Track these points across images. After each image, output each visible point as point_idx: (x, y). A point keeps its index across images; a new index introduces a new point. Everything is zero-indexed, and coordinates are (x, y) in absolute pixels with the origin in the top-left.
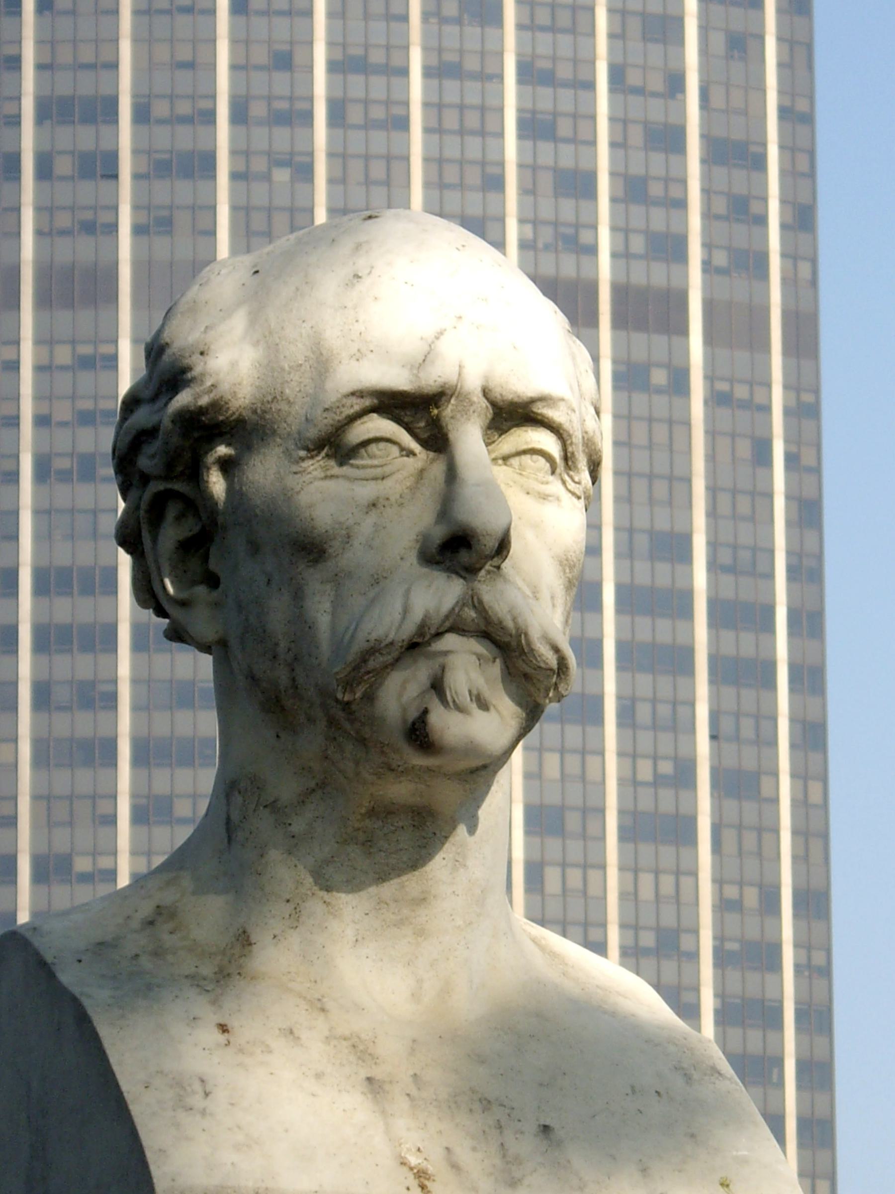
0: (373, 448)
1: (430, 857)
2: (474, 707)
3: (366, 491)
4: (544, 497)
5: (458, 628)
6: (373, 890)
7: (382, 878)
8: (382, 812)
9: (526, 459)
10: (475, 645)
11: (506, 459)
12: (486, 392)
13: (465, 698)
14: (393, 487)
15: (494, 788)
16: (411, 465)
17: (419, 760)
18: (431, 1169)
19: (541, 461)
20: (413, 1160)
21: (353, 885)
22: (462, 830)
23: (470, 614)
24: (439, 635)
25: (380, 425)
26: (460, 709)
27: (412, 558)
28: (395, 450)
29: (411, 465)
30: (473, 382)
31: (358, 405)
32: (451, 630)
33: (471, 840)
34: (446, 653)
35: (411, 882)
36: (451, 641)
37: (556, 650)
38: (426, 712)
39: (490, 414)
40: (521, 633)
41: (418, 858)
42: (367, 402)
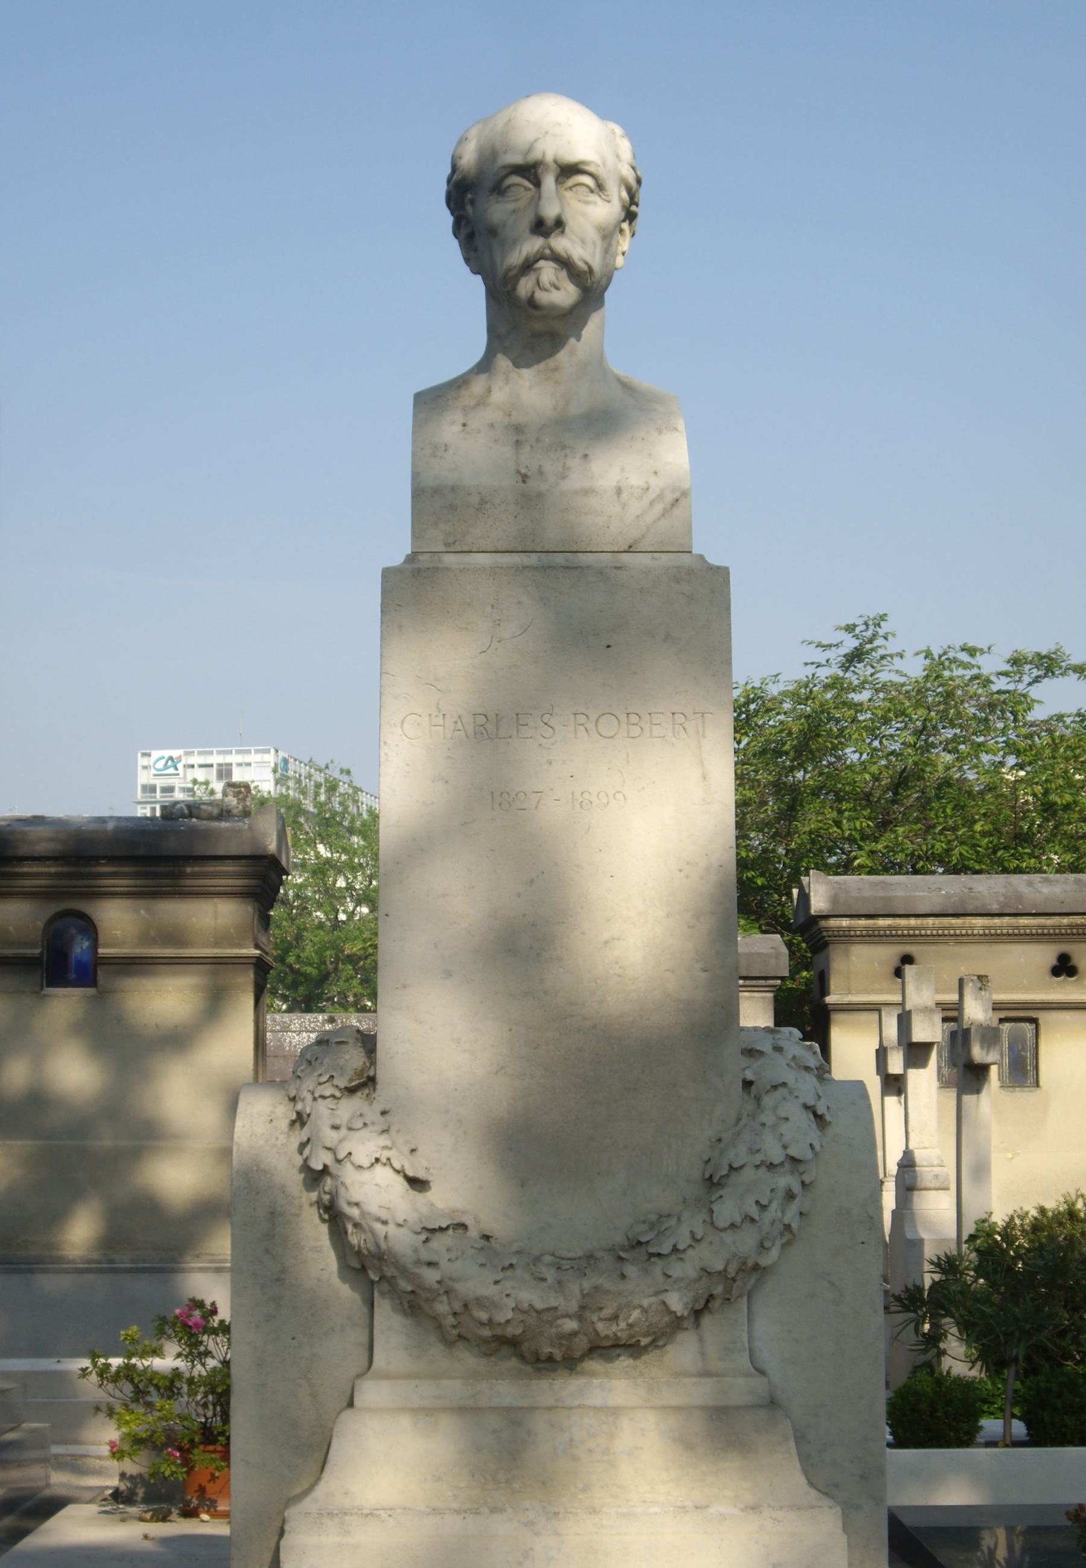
0: (512, 189)
1: (558, 351)
2: (552, 289)
3: (511, 206)
4: (587, 203)
5: (543, 257)
6: (536, 367)
7: (539, 361)
8: (535, 335)
9: (578, 188)
10: (551, 264)
11: (571, 188)
12: (555, 161)
13: (547, 285)
14: (521, 204)
15: (589, 323)
16: (529, 194)
17: (536, 313)
18: (529, 474)
19: (585, 188)
20: (523, 471)
21: (528, 366)
22: (572, 341)
23: (547, 252)
24: (537, 261)
25: (515, 179)
26: (546, 290)
27: (528, 231)
28: (522, 189)
29: (529, 194)
30: (549, 158)
31: (504, 172)
32: (541, 258)
33: (579, 344)
34: (540, 268)
35: (551, 363)
36: (542, 263)
37: (587, 263)
38: (533, 293)
39: (558, 170)
40: (569, 258)
41: (552, 353)
42: (508, 170)
